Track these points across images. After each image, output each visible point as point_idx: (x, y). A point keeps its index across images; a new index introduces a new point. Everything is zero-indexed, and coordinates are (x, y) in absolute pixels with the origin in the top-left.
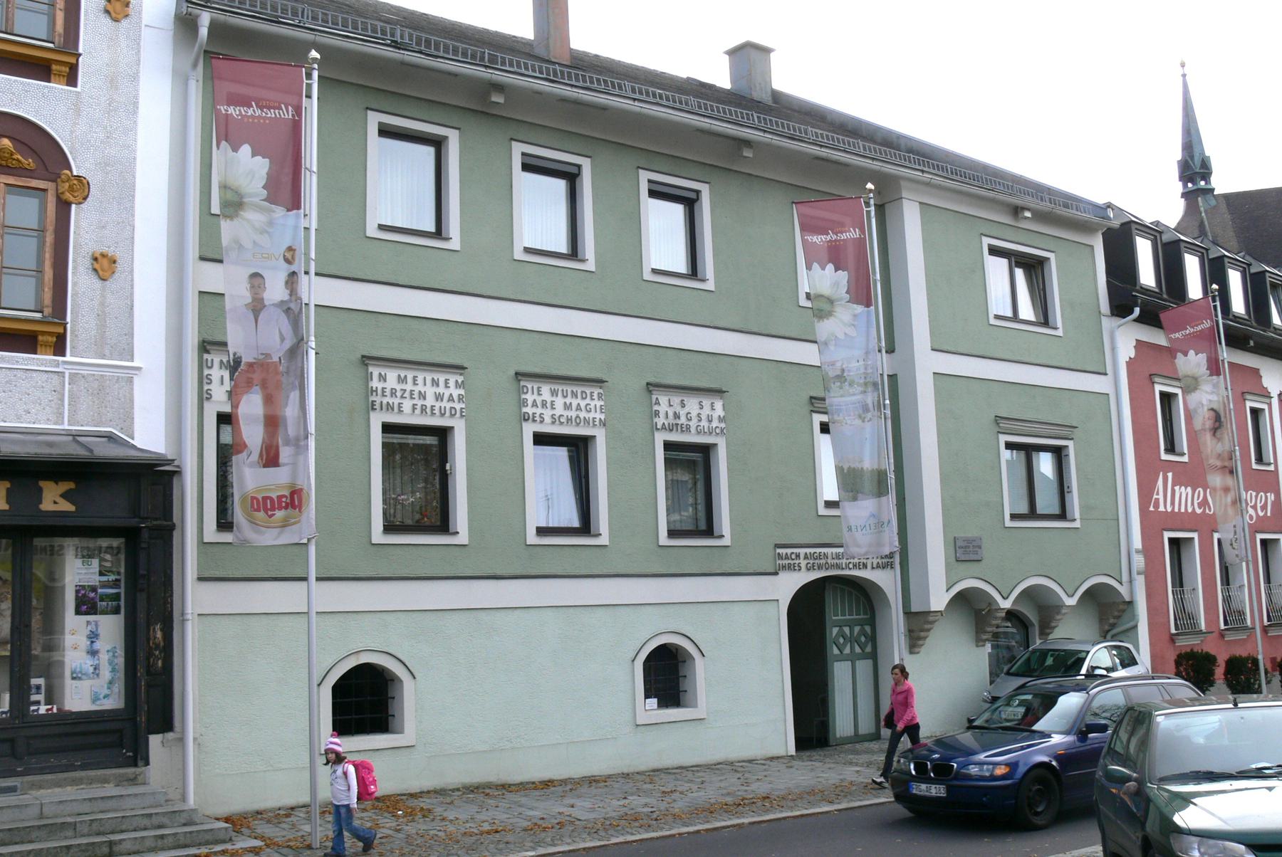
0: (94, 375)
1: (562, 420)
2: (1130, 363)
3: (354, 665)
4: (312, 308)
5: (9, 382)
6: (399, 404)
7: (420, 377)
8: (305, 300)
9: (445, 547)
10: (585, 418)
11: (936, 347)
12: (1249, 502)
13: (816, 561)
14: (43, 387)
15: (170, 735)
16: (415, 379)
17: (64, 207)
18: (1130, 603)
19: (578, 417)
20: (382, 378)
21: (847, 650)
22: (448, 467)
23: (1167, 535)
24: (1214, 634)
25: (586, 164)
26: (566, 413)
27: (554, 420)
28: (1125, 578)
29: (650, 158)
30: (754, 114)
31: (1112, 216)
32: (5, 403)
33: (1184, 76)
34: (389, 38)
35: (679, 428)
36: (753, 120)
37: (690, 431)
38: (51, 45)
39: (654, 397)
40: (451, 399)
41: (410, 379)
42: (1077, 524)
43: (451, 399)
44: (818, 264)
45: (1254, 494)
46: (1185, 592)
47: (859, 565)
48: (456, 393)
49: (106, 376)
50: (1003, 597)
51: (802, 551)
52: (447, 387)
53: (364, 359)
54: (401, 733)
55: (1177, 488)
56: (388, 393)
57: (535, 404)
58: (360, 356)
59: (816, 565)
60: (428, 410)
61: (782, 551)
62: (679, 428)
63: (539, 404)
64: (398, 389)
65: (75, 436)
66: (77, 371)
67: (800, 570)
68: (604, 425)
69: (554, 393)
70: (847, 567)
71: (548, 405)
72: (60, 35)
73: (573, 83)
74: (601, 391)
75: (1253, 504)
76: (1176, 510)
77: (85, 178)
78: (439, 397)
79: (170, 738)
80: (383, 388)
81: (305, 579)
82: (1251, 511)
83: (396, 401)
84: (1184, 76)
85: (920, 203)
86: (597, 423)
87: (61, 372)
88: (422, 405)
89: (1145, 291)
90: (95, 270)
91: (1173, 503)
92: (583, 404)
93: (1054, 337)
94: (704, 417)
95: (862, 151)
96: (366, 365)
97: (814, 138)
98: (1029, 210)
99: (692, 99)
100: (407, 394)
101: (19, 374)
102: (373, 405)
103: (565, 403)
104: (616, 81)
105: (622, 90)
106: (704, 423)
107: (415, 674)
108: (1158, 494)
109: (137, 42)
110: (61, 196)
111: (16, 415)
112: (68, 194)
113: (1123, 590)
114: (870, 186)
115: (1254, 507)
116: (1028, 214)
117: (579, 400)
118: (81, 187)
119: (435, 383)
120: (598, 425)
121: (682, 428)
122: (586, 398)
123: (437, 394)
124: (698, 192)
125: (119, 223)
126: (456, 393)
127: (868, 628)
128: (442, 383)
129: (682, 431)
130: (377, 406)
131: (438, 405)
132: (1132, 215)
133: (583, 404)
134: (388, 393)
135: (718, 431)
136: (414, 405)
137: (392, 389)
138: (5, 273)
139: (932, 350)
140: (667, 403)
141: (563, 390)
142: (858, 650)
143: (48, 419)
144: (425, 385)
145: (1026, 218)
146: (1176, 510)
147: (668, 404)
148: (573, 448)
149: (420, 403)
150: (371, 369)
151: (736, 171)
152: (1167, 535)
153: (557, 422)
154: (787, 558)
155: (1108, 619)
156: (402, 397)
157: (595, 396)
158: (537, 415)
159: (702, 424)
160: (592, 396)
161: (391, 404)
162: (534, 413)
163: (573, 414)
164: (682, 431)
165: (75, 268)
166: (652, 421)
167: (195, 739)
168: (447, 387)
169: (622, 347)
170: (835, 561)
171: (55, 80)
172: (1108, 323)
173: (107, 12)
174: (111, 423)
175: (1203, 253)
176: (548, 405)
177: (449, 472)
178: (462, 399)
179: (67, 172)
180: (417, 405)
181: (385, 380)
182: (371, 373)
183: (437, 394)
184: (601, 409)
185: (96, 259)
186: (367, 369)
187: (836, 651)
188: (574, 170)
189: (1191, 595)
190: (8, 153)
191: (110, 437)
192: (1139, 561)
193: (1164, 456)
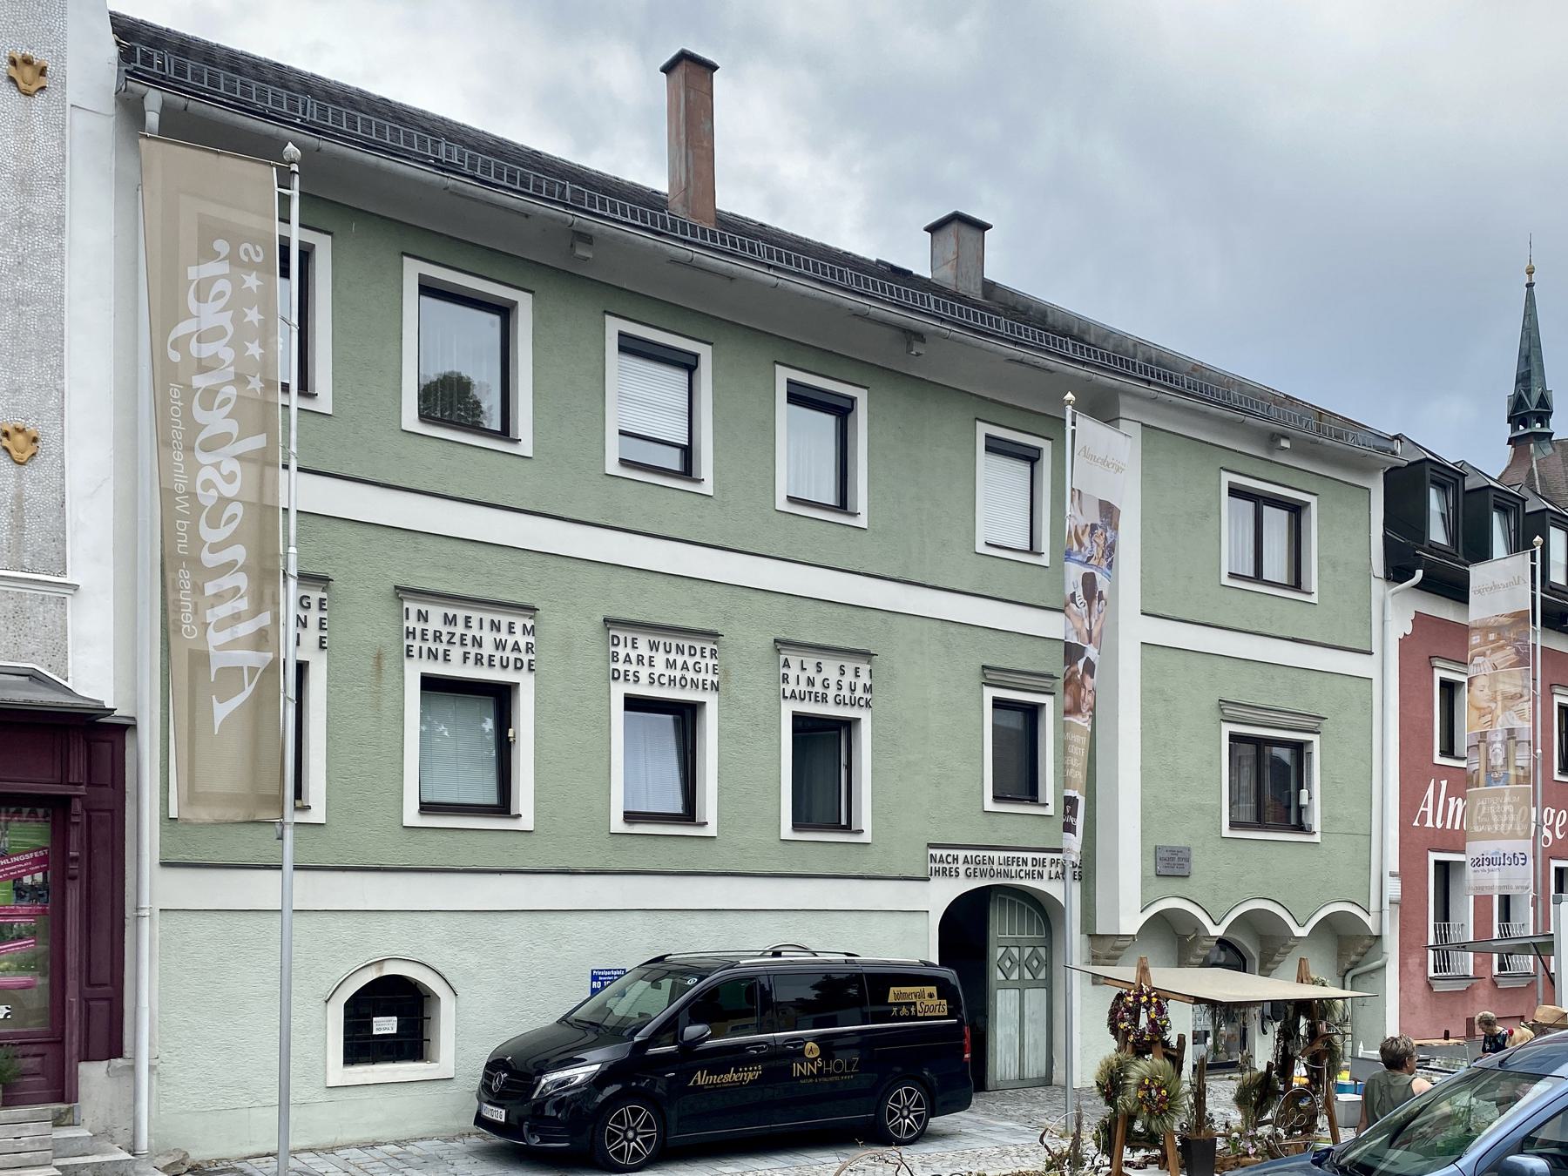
0: (7, 592)
1: (662, 681)
2: (1404, 642)
6: (445, 651)
7: (475, 616)
8: (283, 504)
9: (502, 833)
10: (692, 679)
11: (1146, 611)
12: (1545, 821)
13: (978, 867)
16: (468, 619)
18: (1379, 937)
19: (683, 677)
21: (1015, 976)
22: (511, 734)
23: (1433, 857)
25: (861, 396)
26: (668, 672)
27: (652, 681)
28: (1374, 906)
29: (792, 350)
30: (931, 296)
31: (1399, 451)
33: (1530, 285)
35: (813, 695)
36: (1067, 350)
37: (827, 702)
39: (782, 658)
40: (516, 647)
41: (461, 621)
42: (1317, 838)
43: (516, 647)
45: (1553, 811)
46: (1451, 926)
47: (1033, 874)
48: (523, 641)
50: (1214, 923)
51: (961, 854)
52: (511, 632)
54: (436, 1062)
55: (1452, 800)
56: (430, 636)
57: (628, 660)
59: (978, 871)
60: (485, 661)
61: (937, 852)
62: (813, 695)
63: (634, 659)
67: (957, 876)
68: (717, 689)
69: (653, 646)
70: (1018, 875)
71: (646, 661)
73: (688, 237)
75: (1550, 823)
76: (1449, 826)
78: (500, 645)
80: (626, 671)
82: (1547, 833)
83: (441, 648)
84: (1530, 285)
85: (1143, 424)
86: (708, 686)
88: (477, 654)
89: (1435, 548)
91: (1444, 818)
92: (690, 663)
93: (1240, 592)
94: (845, 684)
95: (1071, 353)
96: (401, 599)
97: (1009, 333)
98: (1286, 438)
99: (849, 271)
100: (456, 639)
102: (408, 651)
103: (668, 659)
104: (957, 305)
105: (843, 281)
106: (845, 692)
107: (457, 990)
108: (1426, 806)
113: (1370, 922)
114: (1069, 396)
115: (1552, 828)
116: (1285, 444)
117: (686, 657)
119: (495, 626)
120: (709, 689)
121: (816, 697)
122: (695, 654)
123: (498, 640)
124: (853, 400)
126: (523, 641)
127: (1042, 951)
128: (504, 628)
129: (816, 701)
130: (415, 652)
131: (498, 654)
132: (1427, 451)
133: (690, 663)
134: (430, 636)
135: (862, 703)
136: (465, 653)
137: (435, 631)
139: (1142, 614)
140: (853, 672)
141: (665, 644)
142: (1028, 976)
144: (481, 628)
145: (1284, 449)
146: (1449, 826)
147: (800, 668)
148: (678, 717)
149: (473, 651)
151: (580, 276)
152: (1433, 857)
153: (656, 682)
154: (941, 861)
155: (1349, 955)
156: (449, 642)
157: (707, 653)
158: (631, 673)
159: (842, 693)
160: (702, 652)
162: (626, 671)
163: (678, 674)
164: (816, 701)
166: (780, 687)
168: (511, 632)
169: (745, 593)
170: (1003, 867)
172: (1379, 587)
174: (33, 658)
175: (1518, 505)
176: (646, 661)
177: (511, 740)
178: (531, 649)
180: (469, 653)
183: (498, 640)
184: (714, 669)
187: (1001, 976)
188: (846, 404)
189: (1458, 932)
191: (34, 677)
192: (1393, 888)
193: (1438, 760)
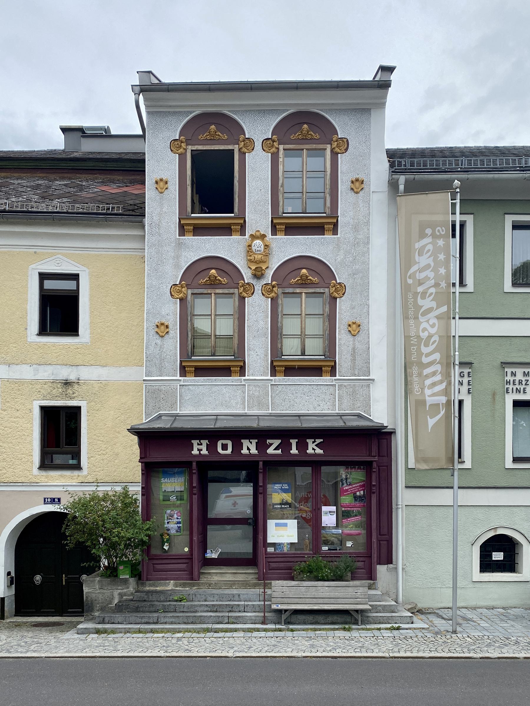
0: (350, 385)
3: (493, 535)
4: (457, 337)
5: (310, 391)
6: (524, 388)
14: (326, 393)
15: (391, 566)
17: (242, 299)
20: (514, 374)
24: (361, 536)
32: (309, 402)
34: (517, 165)
38: (325, 215)
44: (416, 261)
49: (356, 385)
53: (502, 364)
54: (521, 573)
56: (517, 382)
58: (500, 363)
64: (523, 380)
65: (341, 416)
66: (354, 384)
72: (328, 208)
74: (470, 370)
77: (343, 283)
79: (391, 567)
81: (452, 488)
87: (334, 385)
90: (349, 331)
96: (504, 368)
101: (315, 387)
102: (507, 390)
109: (368, 202)
110: (332, 295)
111: (314, 407)
112: (243, 293)
118: (341, 288)
125: (361, 305)
130: (510, 391)
134: (517, 382)
137: (519, 380)
138: (284, 338)
143: (329, 408)
150: (506, 370)
161: (519, 389)
165: (339, 331)
167: (403, 569)
171: (327, 233)
173: (352, 189)
179: (334, 281)
181: (515, 376)
182: (507, 372)
185: (349, 325)
186: (504, 370)
190: (305, 277)
191: (359, 416)
